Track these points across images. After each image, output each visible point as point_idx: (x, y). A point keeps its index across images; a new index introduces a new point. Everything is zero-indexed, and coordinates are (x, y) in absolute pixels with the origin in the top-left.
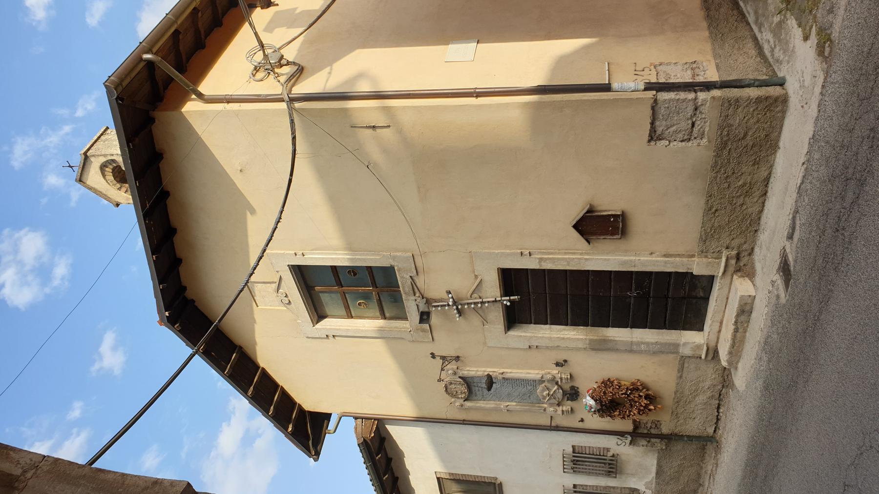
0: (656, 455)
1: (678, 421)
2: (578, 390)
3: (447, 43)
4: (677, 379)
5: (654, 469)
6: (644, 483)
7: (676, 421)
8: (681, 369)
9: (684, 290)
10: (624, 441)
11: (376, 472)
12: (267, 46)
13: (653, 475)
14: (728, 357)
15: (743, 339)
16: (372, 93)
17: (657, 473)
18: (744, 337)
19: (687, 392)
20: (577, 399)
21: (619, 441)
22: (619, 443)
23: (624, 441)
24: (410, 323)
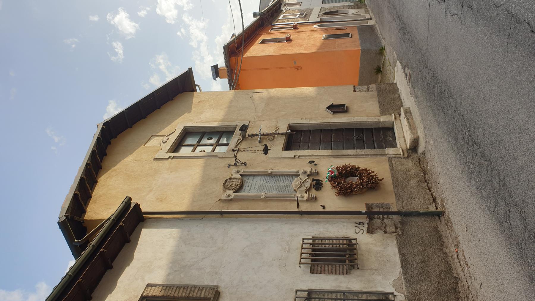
0: (395, 242)
1: (403, 202)
2: (322, 183)
3: (137, 244)
4: (391, 171)
5: (397, 259)
6: (391, 281)
7: (401, 201)
8: (391, 164)
9: (381, 138)
10: (361, 228)
11: (180, 142)
12: (291, 27)
13: (399, 269)
14: (410, 131)
15: (414, 123)
16: (333, 14)
17: (403, 266)
18: (414, 121)
19: (401, 179)
20: (321, 189)
21: (356, 228)
22: (357, 232)
23: (361, 228)
24: (198, 153)
